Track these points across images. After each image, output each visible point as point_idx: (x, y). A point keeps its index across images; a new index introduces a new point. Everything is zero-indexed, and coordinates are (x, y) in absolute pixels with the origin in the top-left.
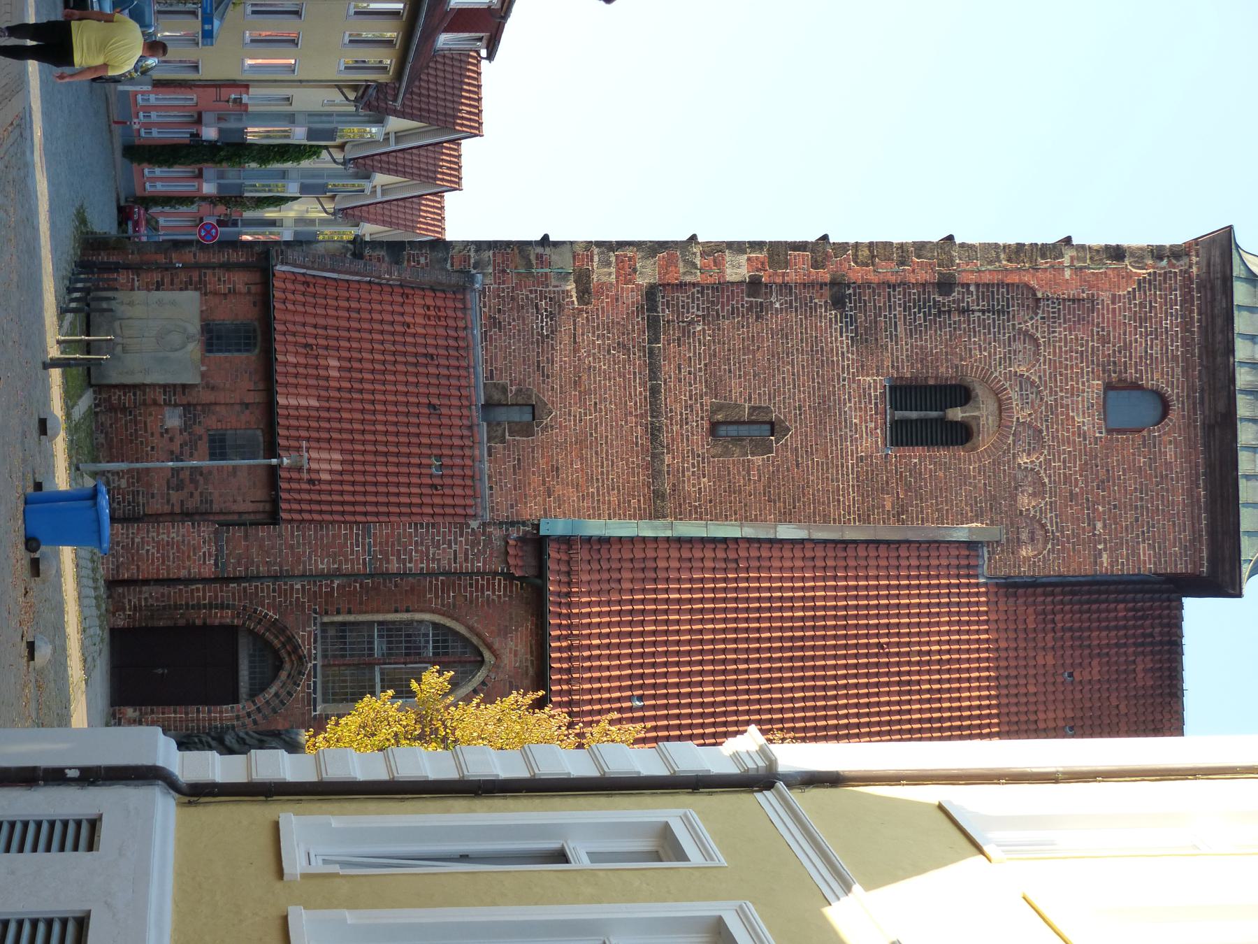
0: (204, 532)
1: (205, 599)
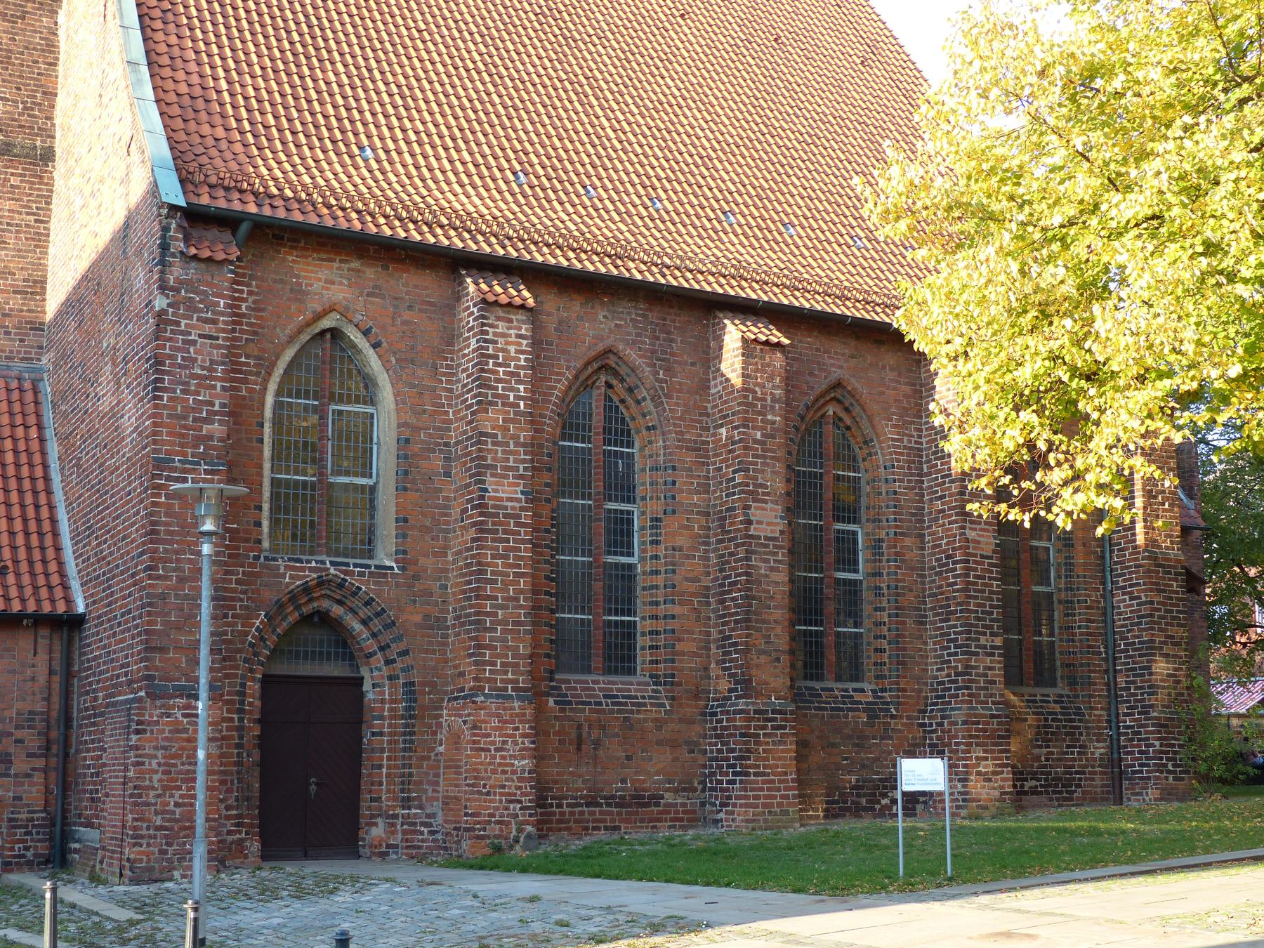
0: (151, 715)
1: (232, 720)
